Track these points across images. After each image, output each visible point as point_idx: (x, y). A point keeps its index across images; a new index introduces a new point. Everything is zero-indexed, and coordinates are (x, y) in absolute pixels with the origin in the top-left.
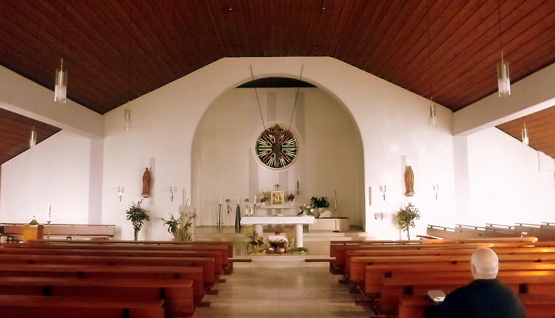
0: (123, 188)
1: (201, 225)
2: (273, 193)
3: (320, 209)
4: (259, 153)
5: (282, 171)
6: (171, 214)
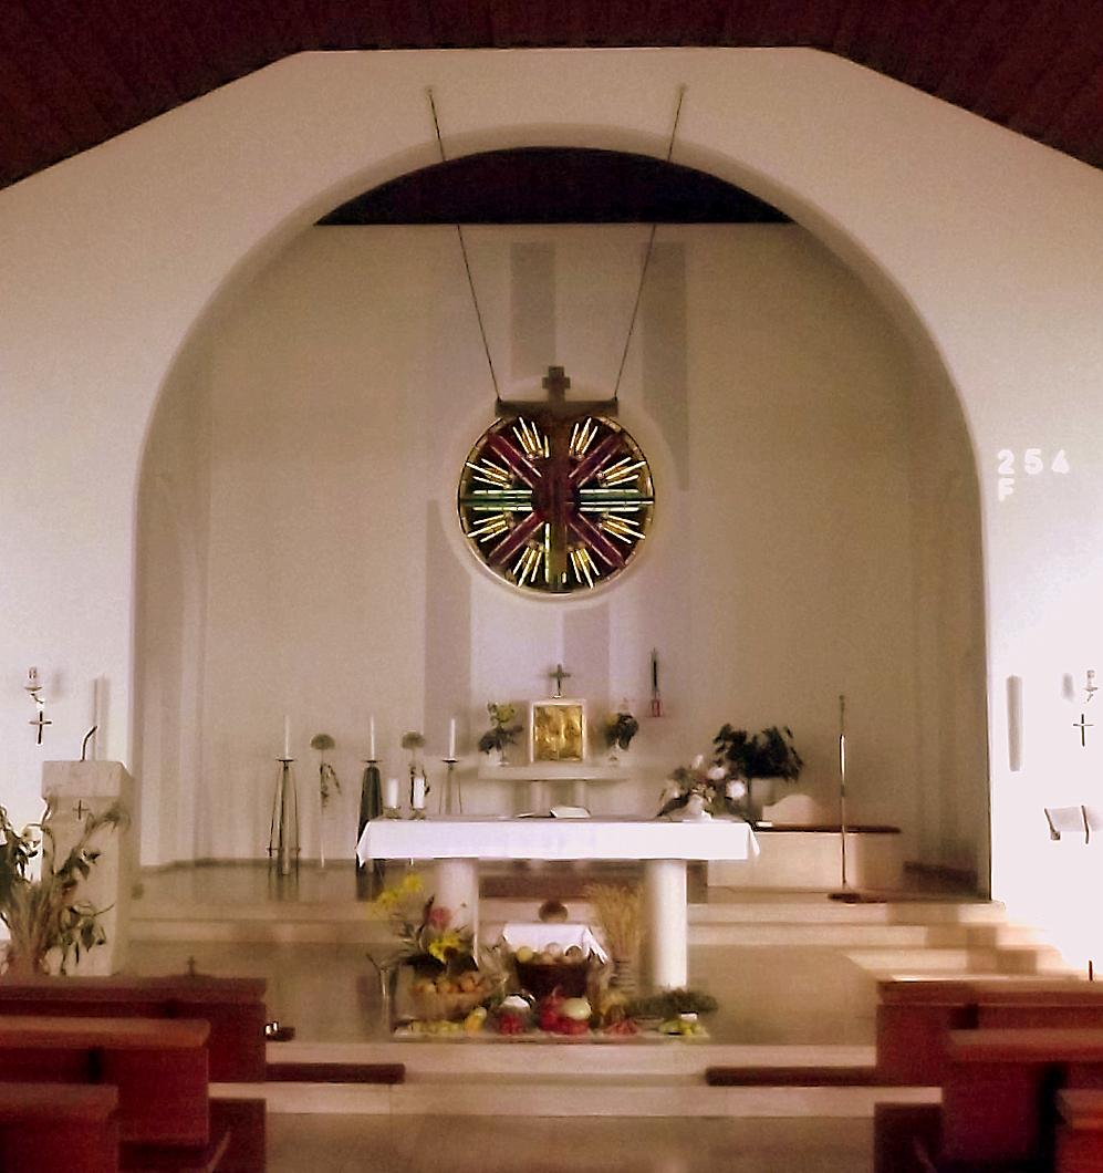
1: (202, 855)
2: (538, 708)
3: (761, 786)
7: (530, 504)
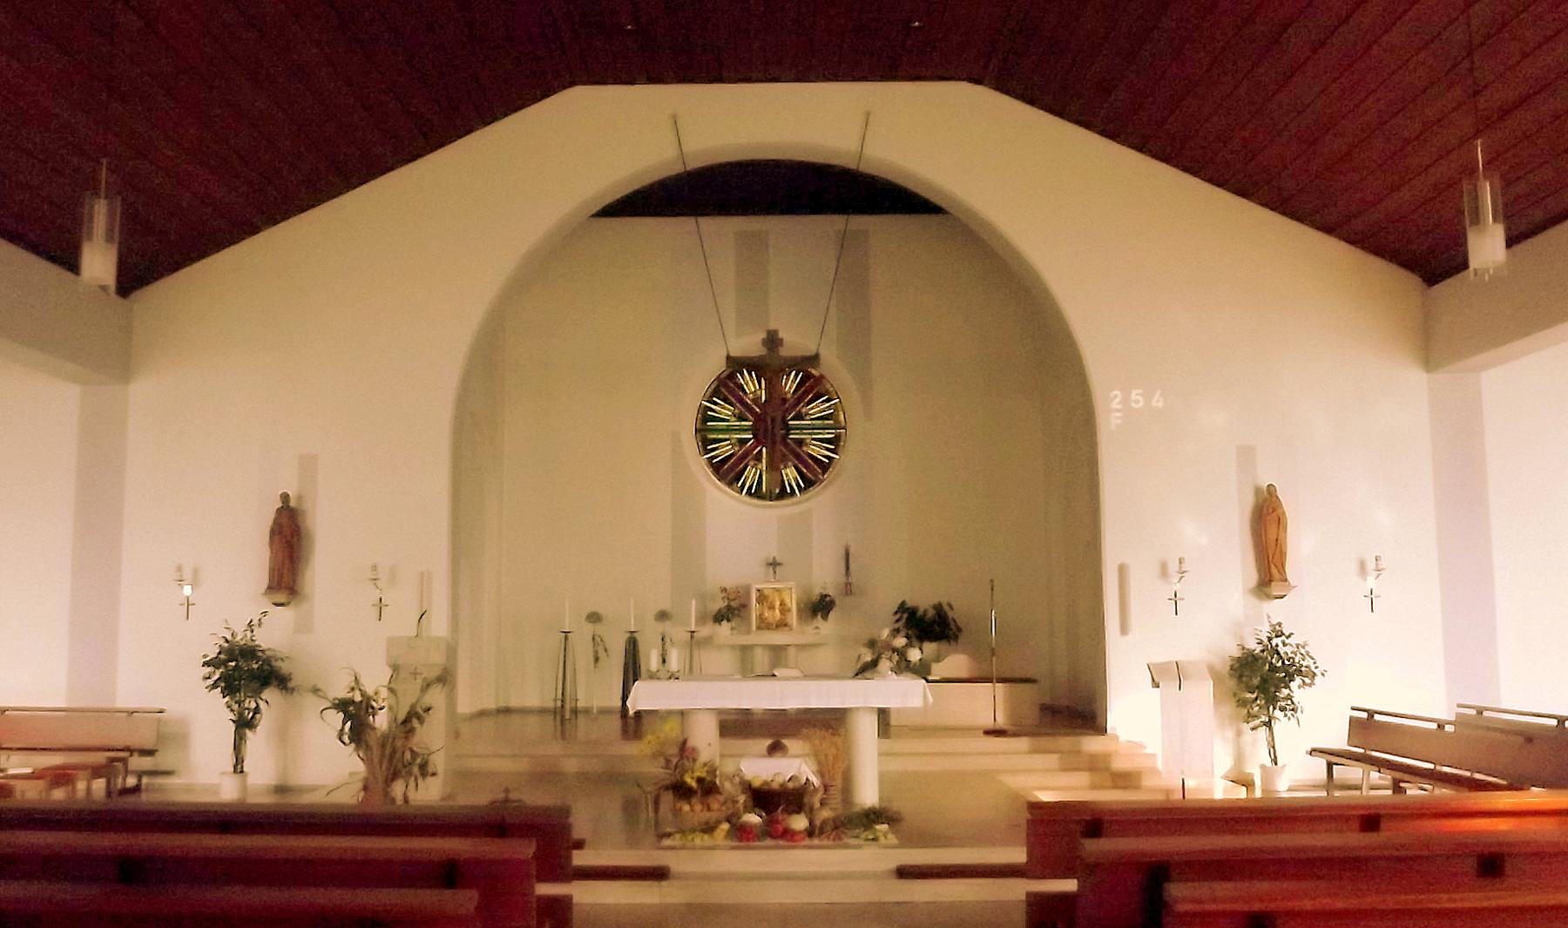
0: (196, 572)
1: (502, 704)
3: (930, 647)
4: (709, 447)
5: (796, 510)
6: (354, 670)
7: (750, 432)
